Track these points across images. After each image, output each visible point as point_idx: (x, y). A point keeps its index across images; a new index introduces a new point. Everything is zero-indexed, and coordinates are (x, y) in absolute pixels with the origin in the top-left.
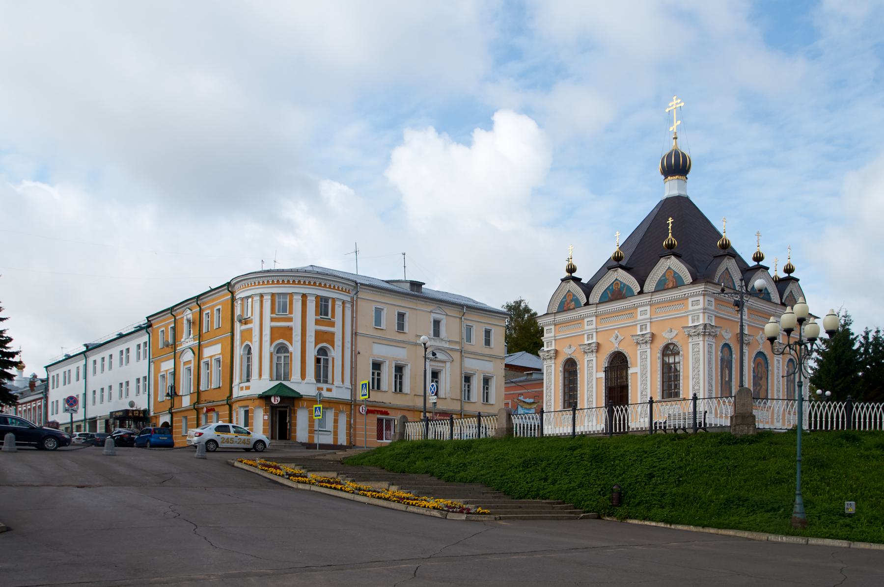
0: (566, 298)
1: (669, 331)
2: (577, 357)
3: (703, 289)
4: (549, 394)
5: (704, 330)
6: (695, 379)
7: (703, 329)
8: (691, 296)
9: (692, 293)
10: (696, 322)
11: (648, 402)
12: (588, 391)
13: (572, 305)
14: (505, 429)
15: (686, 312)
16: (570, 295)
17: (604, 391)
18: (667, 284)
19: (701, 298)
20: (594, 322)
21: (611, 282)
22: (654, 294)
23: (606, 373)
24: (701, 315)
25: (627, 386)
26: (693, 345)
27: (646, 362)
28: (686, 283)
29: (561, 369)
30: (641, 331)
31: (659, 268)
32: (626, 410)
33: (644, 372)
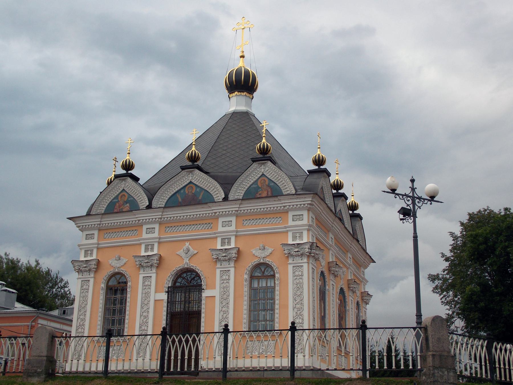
0: (118, 199)
1: (118, 258)
2: (128, 271)
3: (310, 202)
4: (81, 317)
5: (310, 250)
6: (142, 317)
7: (94, 265)
8: (222, 216)
9: (119, 223)
10: (89, 257)
11: (289, 328)
12: (141, 316)
13: (127, 207)
14: (45, 358)
15: (285, 227)
16: (124, 195)
17: (165, 317)
18: (260, 192)
19: (305, 213)
20: (96, 236)
21: (184, 185)
22: (104, 216)
23: (168, 294)
24: (305, 233)
25: (198, 314)
26: (293, 267)
27: (87, 294)
28: (141, 207)
29: (103, 285)
30: (85, 257)
31: (113, 188)
32: (194, 341)
33: (146, 302)
